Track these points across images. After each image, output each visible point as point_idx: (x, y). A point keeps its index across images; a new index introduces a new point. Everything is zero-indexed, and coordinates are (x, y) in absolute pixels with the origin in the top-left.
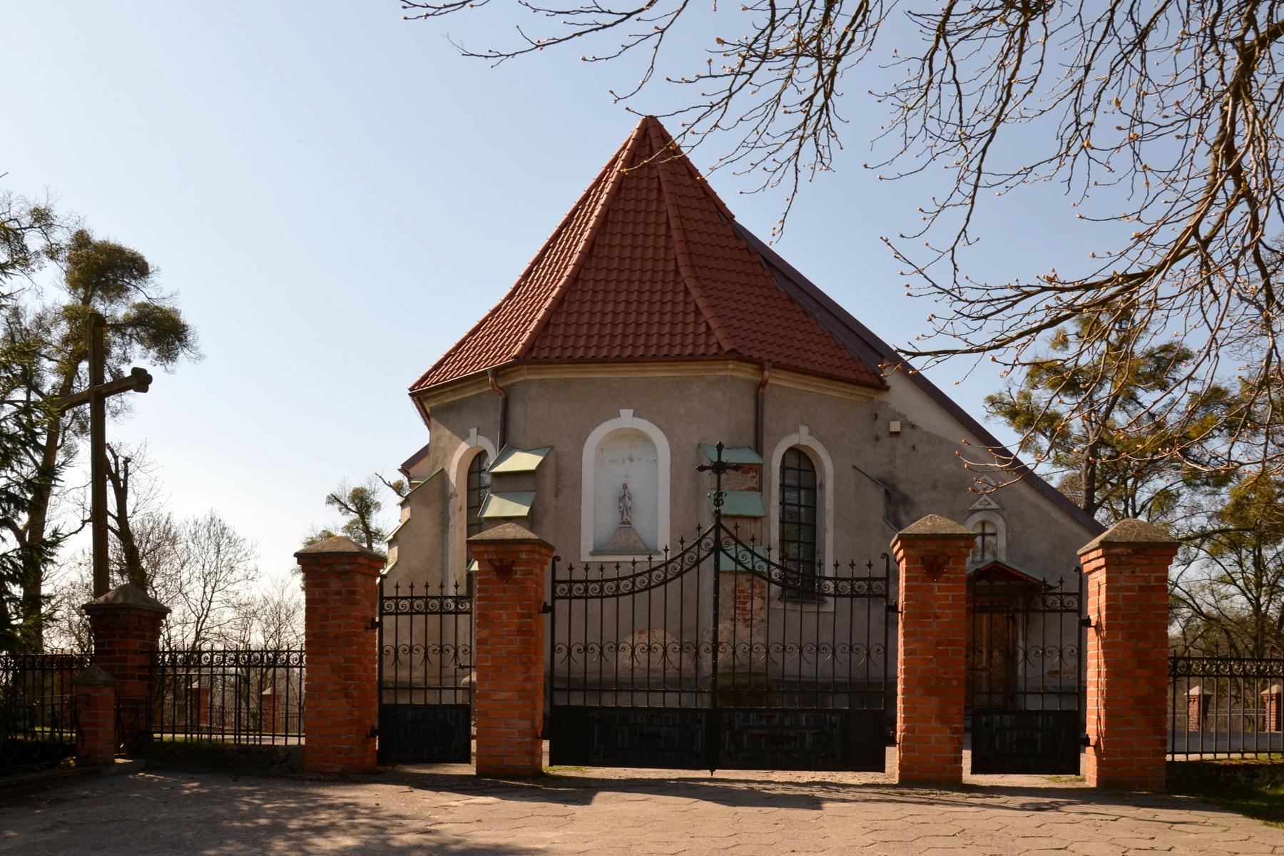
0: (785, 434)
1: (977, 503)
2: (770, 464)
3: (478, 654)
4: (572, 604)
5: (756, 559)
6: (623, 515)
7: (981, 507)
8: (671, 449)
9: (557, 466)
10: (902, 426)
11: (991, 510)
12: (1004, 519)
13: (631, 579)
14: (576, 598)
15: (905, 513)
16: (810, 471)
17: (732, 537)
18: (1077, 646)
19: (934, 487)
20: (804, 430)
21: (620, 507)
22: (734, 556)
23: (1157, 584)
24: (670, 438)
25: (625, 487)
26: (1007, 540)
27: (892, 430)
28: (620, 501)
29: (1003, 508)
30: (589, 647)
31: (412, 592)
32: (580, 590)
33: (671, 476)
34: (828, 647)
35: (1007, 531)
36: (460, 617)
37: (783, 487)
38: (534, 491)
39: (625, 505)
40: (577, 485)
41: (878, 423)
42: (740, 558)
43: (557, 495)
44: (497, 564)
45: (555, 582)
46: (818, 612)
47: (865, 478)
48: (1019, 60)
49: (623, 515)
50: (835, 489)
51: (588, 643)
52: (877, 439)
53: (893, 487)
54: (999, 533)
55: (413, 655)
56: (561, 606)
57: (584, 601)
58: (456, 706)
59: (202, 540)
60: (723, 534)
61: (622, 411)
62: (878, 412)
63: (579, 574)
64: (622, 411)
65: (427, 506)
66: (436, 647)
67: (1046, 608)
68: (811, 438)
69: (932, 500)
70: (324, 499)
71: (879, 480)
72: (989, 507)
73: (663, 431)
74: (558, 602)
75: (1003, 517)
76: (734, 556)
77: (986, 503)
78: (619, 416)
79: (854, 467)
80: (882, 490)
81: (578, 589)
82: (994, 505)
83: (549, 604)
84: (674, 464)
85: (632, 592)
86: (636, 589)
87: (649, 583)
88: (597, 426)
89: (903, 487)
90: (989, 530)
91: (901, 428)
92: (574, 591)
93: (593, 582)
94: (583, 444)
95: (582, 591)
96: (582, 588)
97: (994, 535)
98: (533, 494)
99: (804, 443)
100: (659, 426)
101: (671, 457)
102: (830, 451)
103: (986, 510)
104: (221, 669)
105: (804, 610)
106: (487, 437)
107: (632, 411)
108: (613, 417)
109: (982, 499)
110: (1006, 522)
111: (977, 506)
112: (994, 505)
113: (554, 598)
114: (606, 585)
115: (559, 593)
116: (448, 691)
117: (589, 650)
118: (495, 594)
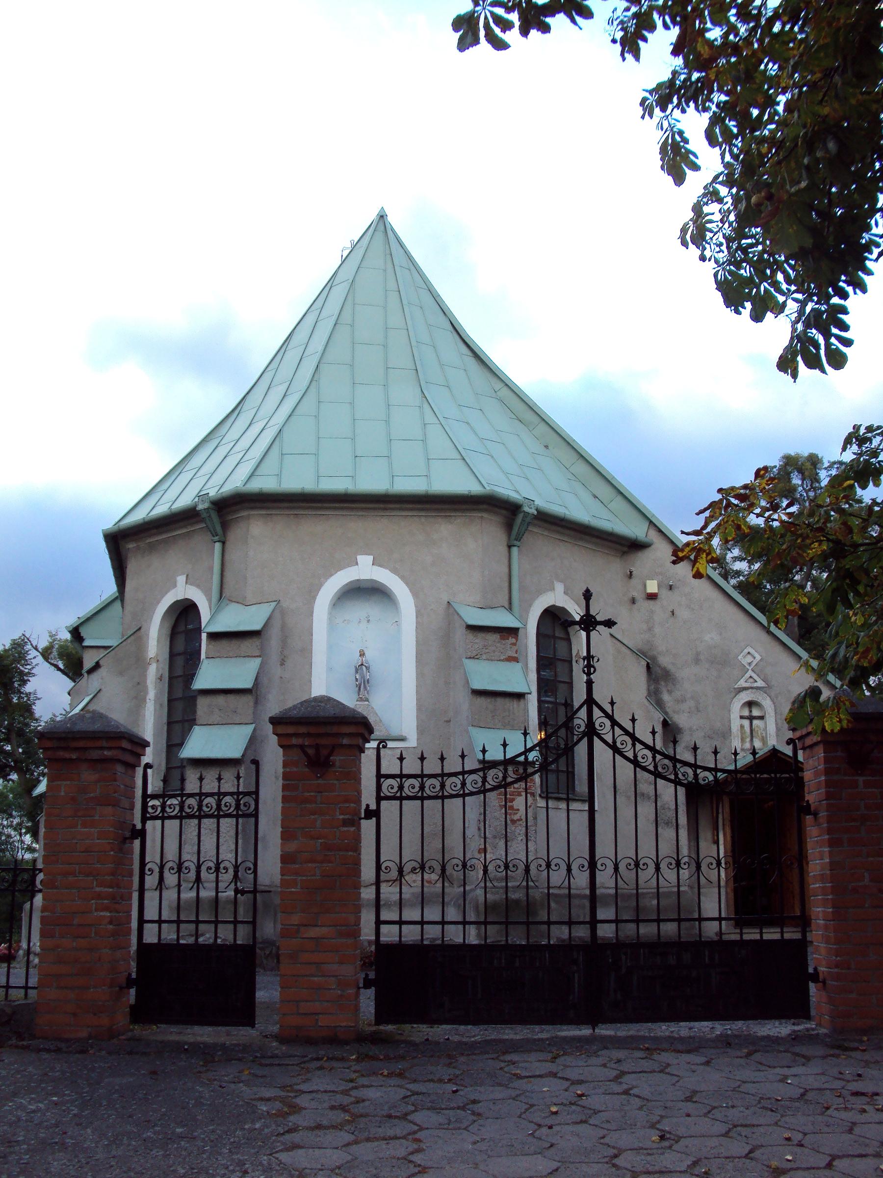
0: (540, 592)
1: (742, 680)
3: (282, 875)
4: (404, 806)
5: (639, 746)
6: (359, 689)
8: (416, 606)
9: (283, 627)
10: (659, 586)
11: (758, 688)
12: (772, 701)
13: (481, 774)
14: (409, 798)
15: (668, 690)
17: (607, 716)
18: (588, 857)
19: (697, 661)
20: (559, 587)
21: (357, 680)
22: (610, 741)
23: (856, 778)
24: (415, 594)
25: (362, 654)
26: (777, 724)
27: (649, 590)
28: (357, 672)
29: (769, 687)
30: (641, 863)
31: (201, 787)
32: (413, 788)
33: (417, 641)
34: (649, 862)
35: (776, 713)
36: (205, 821)
38: (260, 656)
39: (363, 677)
40: (306, 651)
41: (634, 581)
42: (619, 745)
43: (282, 663)
44: (311, 752)
45: (379, 776)
47: (624, 649)
49: (359, 689)
51: (425, 860)
52: (633, 601)
53: (654, 658)
54: (767, 716)
55: (220, 875)
56: (389, 809)
57: (419, 802)
58: (235, 947)
60: (597, 712)
61: (360, 558)
62: (633, 569)
63: (411, 766)
64: (360, 558)
65: (121, 673)
66: (630, 861)
67: (240, 813)
68: (566, 597)
69: (695, 675)
71: (640, 651)
72: (755, 685)
73: (407, 584)
74: (384, 804)
75: (770, 697)
76: (610, 741)
77: (751, 680)
78: (357, 564)
80: (644, 663)
83: (373, 807)
84: (420, 625)
85: (483, 791)
86: (488, 786)
87: (505, 778)
88: (331, 575)
89: (665, 661)
90: (756, 712)
91: (658, 589)
92: (406, 790)
93: (409, 776)
94: (314, 598)
95: (417, 789)
96: (417, 785)
97: (761, 718)
98: (258, 661)
99: (559, 604)
100: (402, 578)
101: (417, 617)
103: (752, 688)
106: (198, 586)
108: (349, 566)
109: (747, 675)
110: (774, 703)
111: (742, 683)
112: (760, 683)
113: (379, 799)
114: (449, 782)
115: (385, 791)
116: (606, 925)
117: (553, 867)
118: (306, 794)
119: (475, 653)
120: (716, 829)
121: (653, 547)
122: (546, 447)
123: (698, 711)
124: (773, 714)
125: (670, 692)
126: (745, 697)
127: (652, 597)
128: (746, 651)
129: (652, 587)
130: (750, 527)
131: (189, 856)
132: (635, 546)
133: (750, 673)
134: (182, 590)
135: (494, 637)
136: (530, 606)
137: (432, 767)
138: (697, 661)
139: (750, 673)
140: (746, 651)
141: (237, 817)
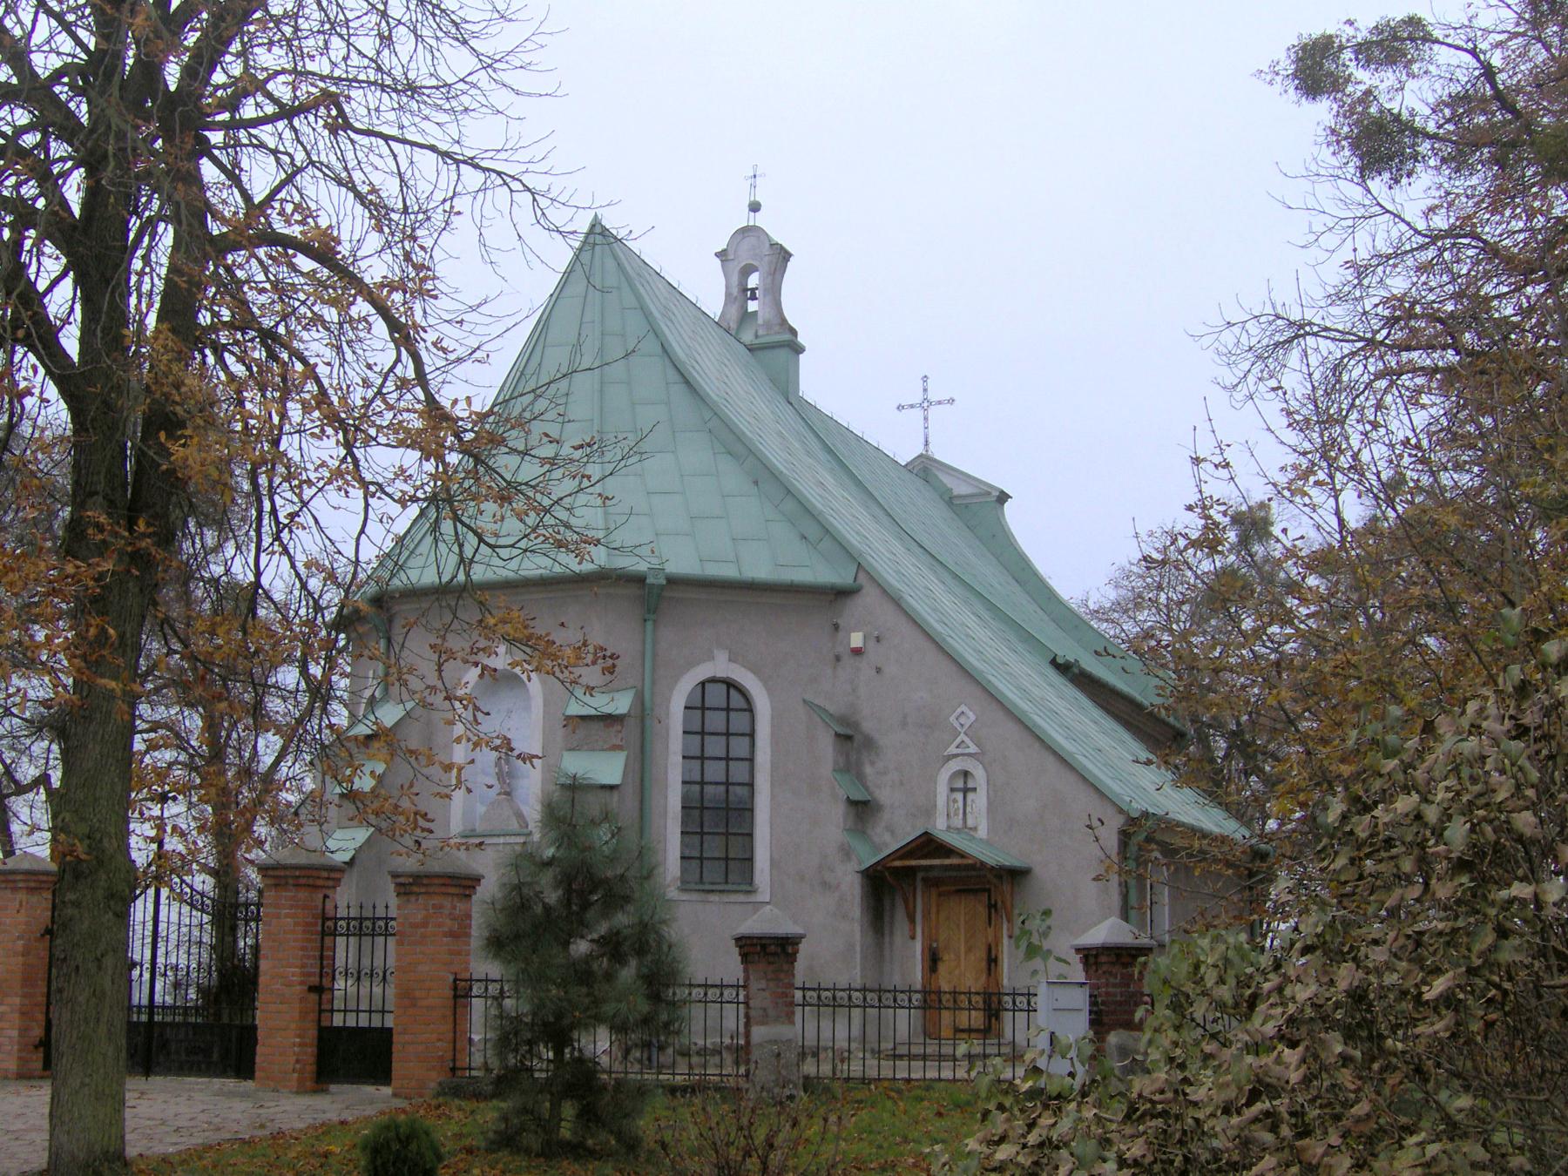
0: (691, 664)
2: (668, 708)
7: (959, 751)
11: (969, 755)
16: (745, 710)
26: (988, 798)
27: (853, 645)
37: (752, 735)
46: (738, 986)
48: (1458, 48)
50: (773, 734)
52: (838, 658)
59: (1166, 1043)
70: (1279, 48)
72: (967, 751)
79: (804, 701)
81: (888, 999)
82: (973, 749)
102: (765, 681)
104: (202, 423)
105: (318, 979)
107: (648, 581)
109: (958, 740)
111: (952, 750)
112: (973, 749)
119: (575, 744)
120: (912, 919)
121: (864, 591)
122: (756, 483)
123: (902, 783)
124: (984, 786)
125: (872, 763)
126: (954, 766)
127: (857, 652)
128: (959, 710)
129: (856, 640)
130: (1322, 561)
131: (379, 962)
132: (841, 594)
133: (962, 737)
134: (721, 666)
135: (596, 727)
136: (676, 682)
137: (368, 913)
138: (904, 724)
139: (962, 737)
140: (959, 710)
141: (348, 935)
